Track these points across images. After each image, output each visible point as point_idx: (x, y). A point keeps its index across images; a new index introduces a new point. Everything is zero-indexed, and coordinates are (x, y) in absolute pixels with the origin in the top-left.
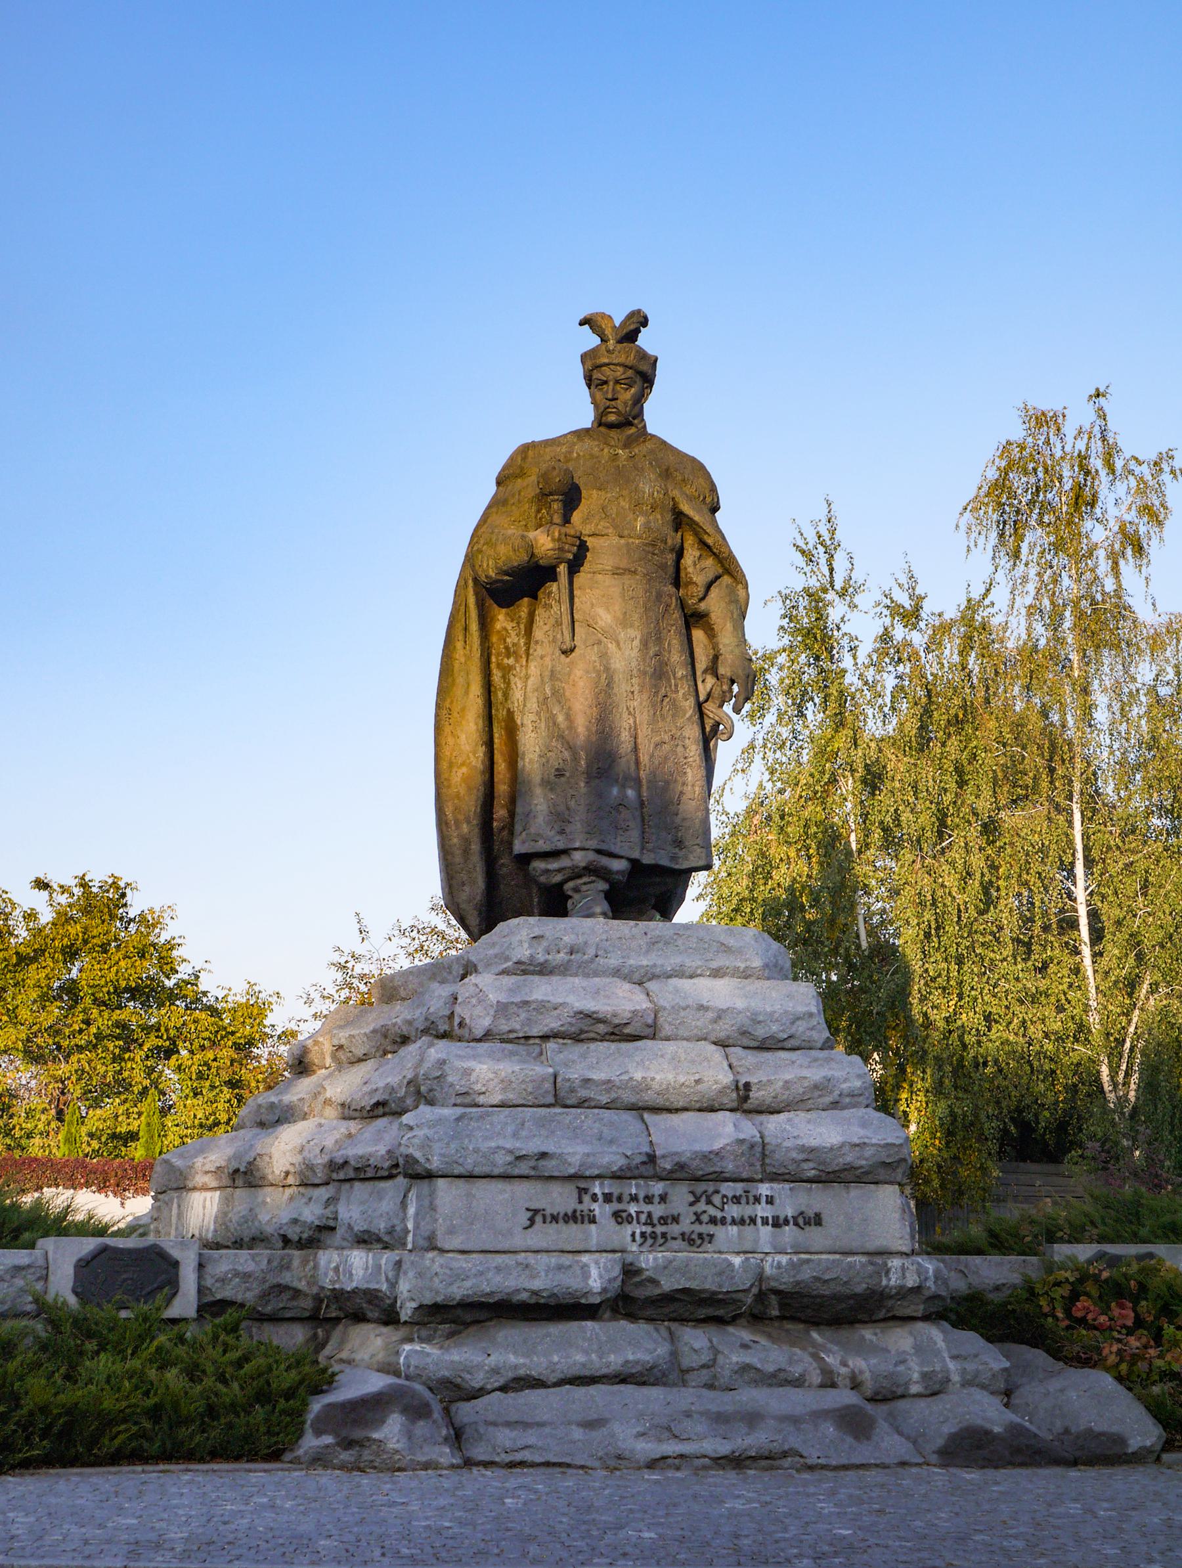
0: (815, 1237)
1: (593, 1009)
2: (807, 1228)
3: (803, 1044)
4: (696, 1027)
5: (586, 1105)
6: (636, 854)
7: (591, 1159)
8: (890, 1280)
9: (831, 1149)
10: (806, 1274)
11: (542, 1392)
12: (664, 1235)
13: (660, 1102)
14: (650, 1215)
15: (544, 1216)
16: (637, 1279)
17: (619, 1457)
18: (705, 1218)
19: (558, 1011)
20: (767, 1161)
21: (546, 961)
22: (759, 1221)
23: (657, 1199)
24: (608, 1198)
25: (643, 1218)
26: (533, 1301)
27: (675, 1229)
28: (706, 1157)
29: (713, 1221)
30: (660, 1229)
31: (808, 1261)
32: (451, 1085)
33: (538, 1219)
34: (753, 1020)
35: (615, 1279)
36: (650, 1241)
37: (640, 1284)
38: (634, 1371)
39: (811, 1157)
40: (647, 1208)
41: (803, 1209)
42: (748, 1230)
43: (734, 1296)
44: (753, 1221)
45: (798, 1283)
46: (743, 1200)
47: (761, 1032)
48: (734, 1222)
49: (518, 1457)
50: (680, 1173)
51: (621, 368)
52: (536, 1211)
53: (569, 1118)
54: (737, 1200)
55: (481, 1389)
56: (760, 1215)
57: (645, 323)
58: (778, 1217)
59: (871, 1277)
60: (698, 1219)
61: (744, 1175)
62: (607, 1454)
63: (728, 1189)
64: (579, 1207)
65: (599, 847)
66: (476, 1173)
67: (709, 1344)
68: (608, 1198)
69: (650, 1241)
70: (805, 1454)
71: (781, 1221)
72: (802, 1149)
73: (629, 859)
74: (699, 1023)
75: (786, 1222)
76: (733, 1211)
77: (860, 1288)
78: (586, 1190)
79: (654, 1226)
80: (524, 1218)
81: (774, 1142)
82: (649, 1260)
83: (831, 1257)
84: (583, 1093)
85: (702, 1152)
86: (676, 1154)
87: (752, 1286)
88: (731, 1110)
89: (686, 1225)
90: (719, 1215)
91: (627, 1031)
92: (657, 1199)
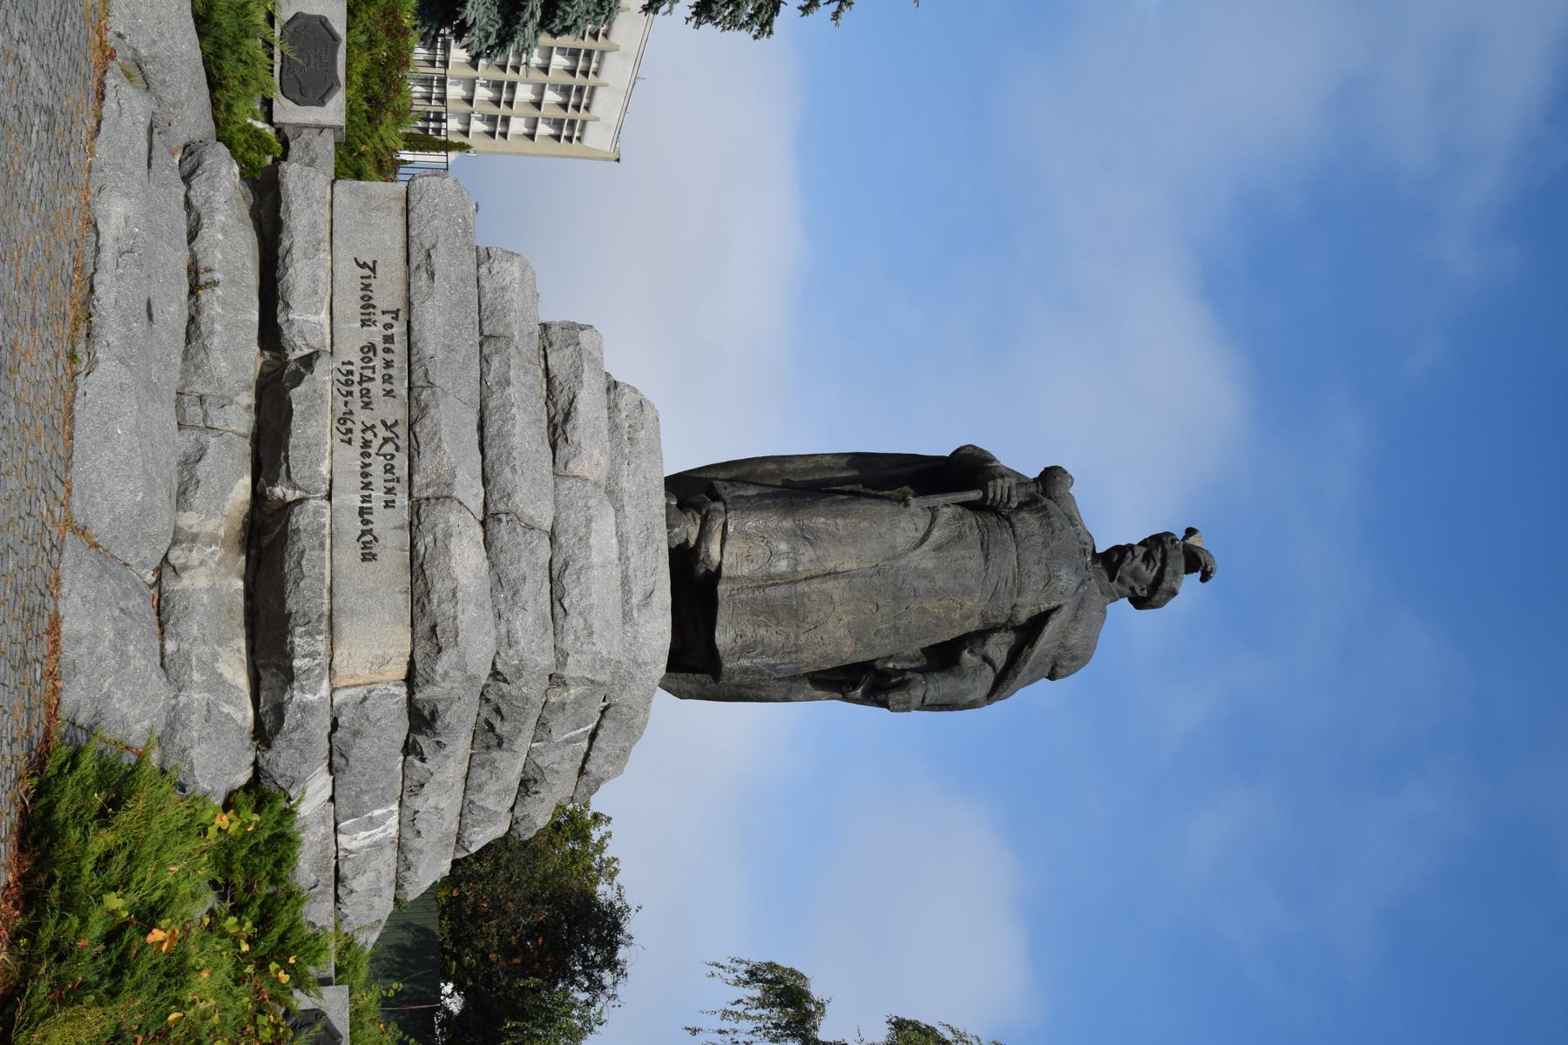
0: (349, 554)
12: (350, 393)
13: (491, 431)
14: (371, 379)
22: (366, 493)
23: (388, 387)
25: (368, 373)
27: (356, 403)
29: (366, 444)
30: (356, 389)
31: (322, 546)
33: (367, 272)
36: (343, 379)
42: (358, 481)
44: (367, 486)
46: (389, 476)
47: (568, 580)
48: (365, 465)
52: (373, 270)
54: (389, 469)
59: (304, 615)
61: (416, 478)
63: (401, 461)
64: (378, 312)
68: (389, 339)
75: (366, 522)
77: (291, 604)
79: (360, 383)
82: (323, 376)
89: (361, 416)
90: (372, 451)
92: (388, 387)
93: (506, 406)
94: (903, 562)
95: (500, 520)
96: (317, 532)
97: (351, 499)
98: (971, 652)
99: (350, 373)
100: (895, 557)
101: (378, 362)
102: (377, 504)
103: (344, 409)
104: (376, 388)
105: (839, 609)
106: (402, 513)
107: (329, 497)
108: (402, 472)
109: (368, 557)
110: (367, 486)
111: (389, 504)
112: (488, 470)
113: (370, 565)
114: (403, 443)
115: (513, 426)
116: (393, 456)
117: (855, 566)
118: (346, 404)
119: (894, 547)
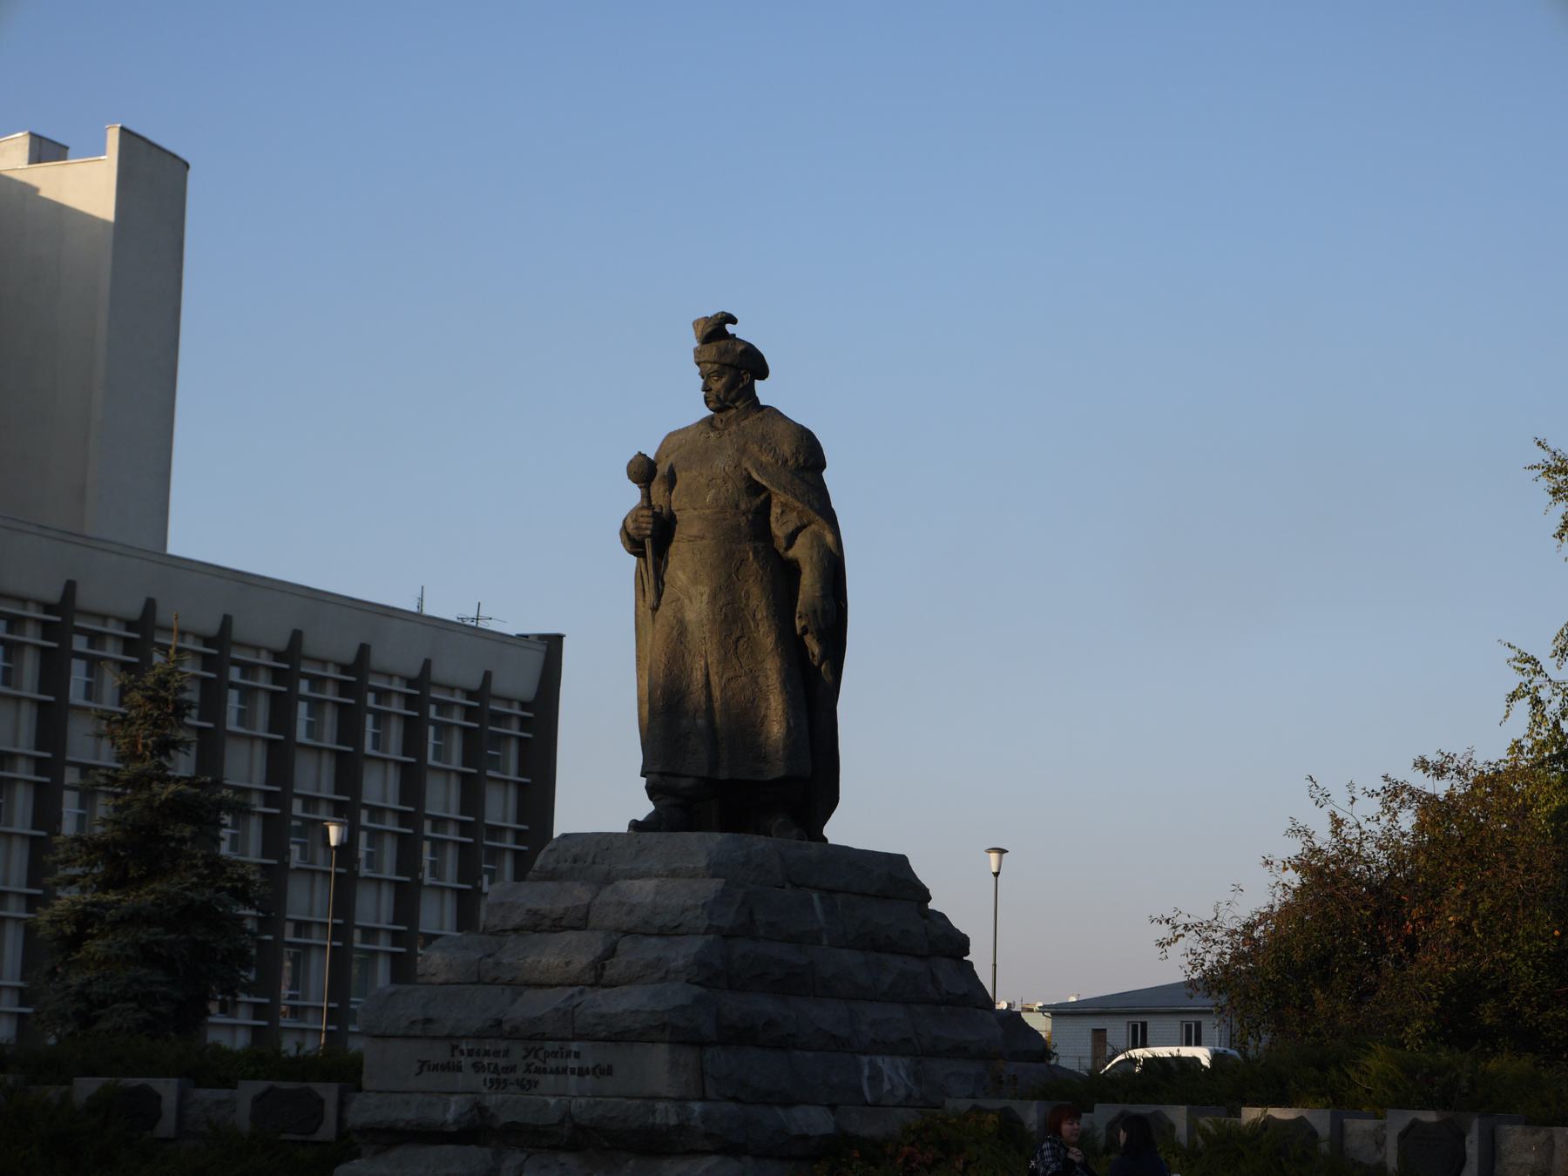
27: (512, 1077)
30: (503, 1076)
40: (495, 1060)
51: (732, 365)
54: (555, 1054)
63: (551, 1046)
68: (470, 1053)
76: (552, 1063)
82: (492, 1100)
89: (519, 1074)
104: (502, 1062)
110: (564, 1070)
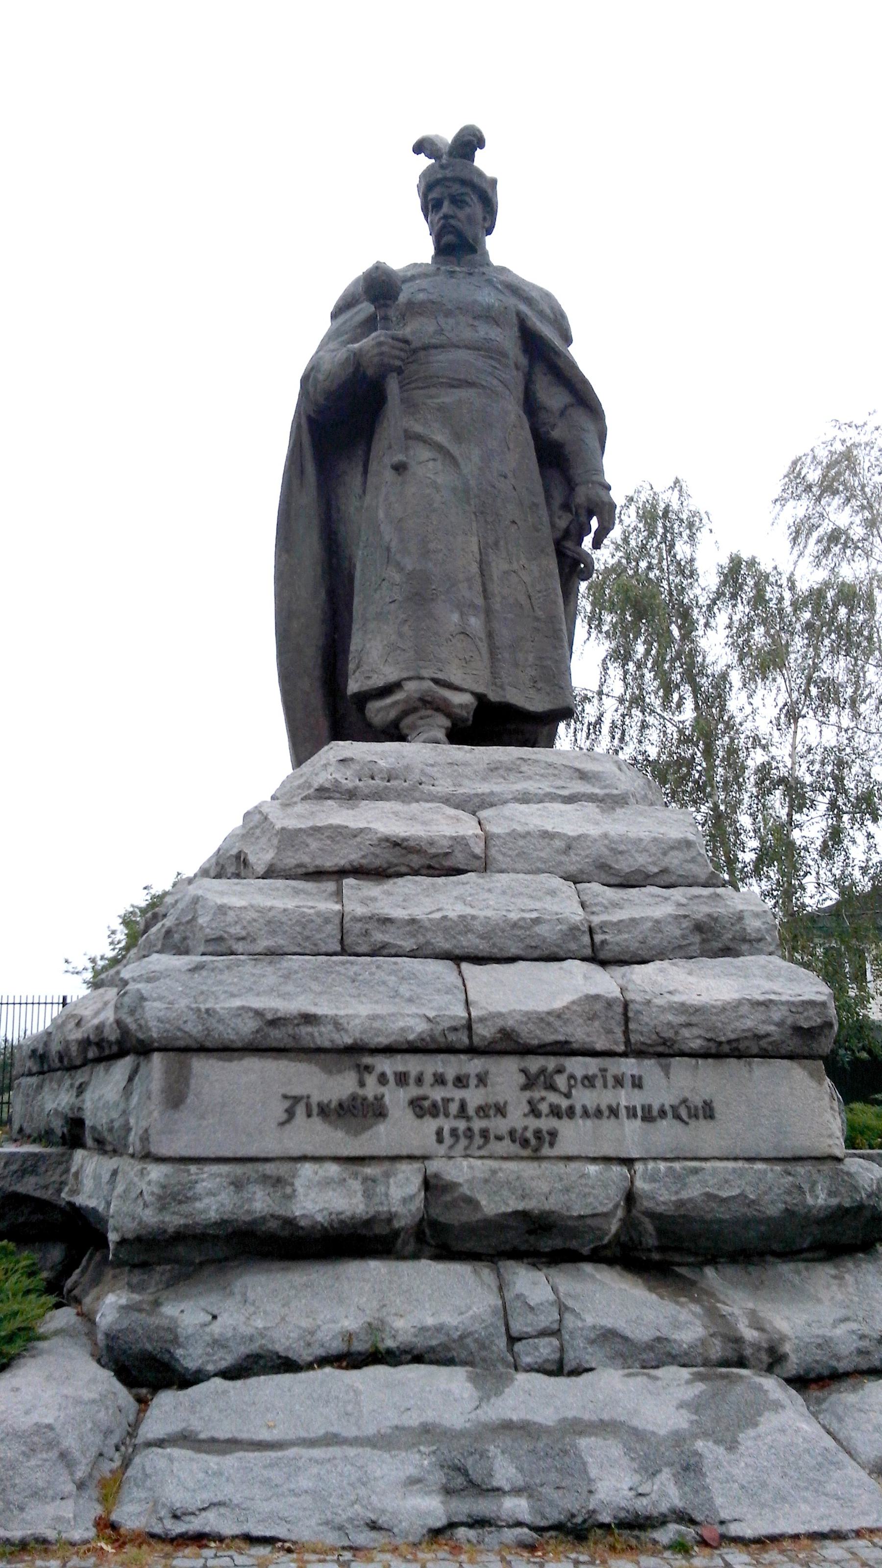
0: (704, 1137)
1: (403, 834)
2: (693, 1123)
3: (681, 880)
4: (540, 859)
5: (385, 952)
6: (481, 689)
7: (377, 1024)
8: (817, 1197)
9: (724, 1009)
10: (693, 1191)
11: (286, 1379)
12: (485, 1134)
13: (483, 947)
14: (463, 1106)
15: (308, 1106)
16: (448, 1198)
17: (373, 1526)
18: (544, 1108)
19: (358, 839)
20: (632, 1026)
21: (356, 788)
22: (623, 1112)
23: (473, 1081)
24: (402, 1079)
25: (454, 1108)
26: (286, 1233)
27: (499, 1125)
28: (543, 1019)
29: (556, 1112)
30: (477, 1125)
31: (696, 1171)
32: (202, 928)
33: (300, 1110)
34: (612, 850)
35: (412, 1198)
36: (463, 1142)
37: (454, 1204)
38: (434, 1343)
39: (694, 1019)
40: (458, 1094)
41: (687, 1095)
42: (608, 1125)
43: (589, 1221)
44: (614, 1112)
45: (681, 1203)
46: (599, 1083)
47: (624, 865)
48: (586, 1113)
49: (194, 1525)
50: (508, 1044)
51: (458, 194)
52: (296, 1100)
53: (355, 968)
54: (589, 1081)
55: (199, 1371)
56: (623, 1103)
57: (480, 142)
58: (650, 1106)
59: (789, 1193)
60: (535, 1112)
61: (599, 1046)
62: (351, 1520)
63: (577, 1066)
64: (361, 1092)
65: (436, 676)
66: (208, 1044)
67: (552, 1297)
68: (402, 1079)
69: (463, 1142)
70: (699, 1518)
71: (655, 1113)
72: (683, 1009)
73: (473, 693)
74: (542, 854)
75: (663, 1113)
76: (584, 1097)
77: (774, 1210)
78: (368, 1069)
79: (468, 1119)
80: (278, 1109)
81: (638, 998)
82: (462, 1171)
83: (731, 1165)
84: (379, 937)
85: (536, 1012)
86: (500, 1015)
87: (616, 1206)
88: (583, 959)
89: (517, 1117)
90: (564, 1103)
91: (447, 863)
92: (473, 1081)
93: (445, 925)
94: (472, 483)
95: (603, 942)
96: (679, 1178)
97: (630, 1136)
98: (554, 426)
99: (454, 1132)
100: (467, 491)
101: (437, 1094)
102: (637, 1099)
103: (507, 1141)
104: (474, 1097)
105: (515, 566)
106: (648, 1068)
107: (628, 1162)
108: (592, 1065)
109: (708, 1111)
110: (614, 1112)
111: (637, 1083)
112: (537, 953)
113: (718, 1107)
114: (551, 1063)
115: (474, 918)
116: (572, 1077)
117: (475, 539)
118: (499, 1138)
119: (454, 490)
